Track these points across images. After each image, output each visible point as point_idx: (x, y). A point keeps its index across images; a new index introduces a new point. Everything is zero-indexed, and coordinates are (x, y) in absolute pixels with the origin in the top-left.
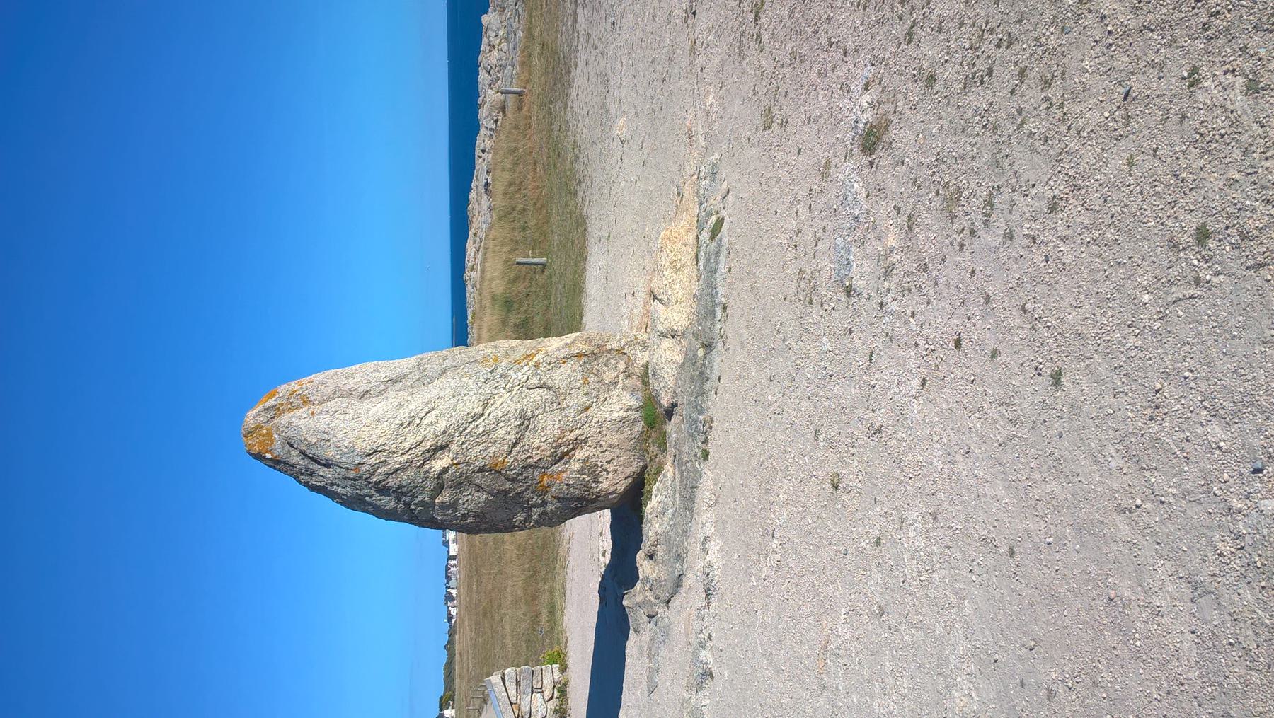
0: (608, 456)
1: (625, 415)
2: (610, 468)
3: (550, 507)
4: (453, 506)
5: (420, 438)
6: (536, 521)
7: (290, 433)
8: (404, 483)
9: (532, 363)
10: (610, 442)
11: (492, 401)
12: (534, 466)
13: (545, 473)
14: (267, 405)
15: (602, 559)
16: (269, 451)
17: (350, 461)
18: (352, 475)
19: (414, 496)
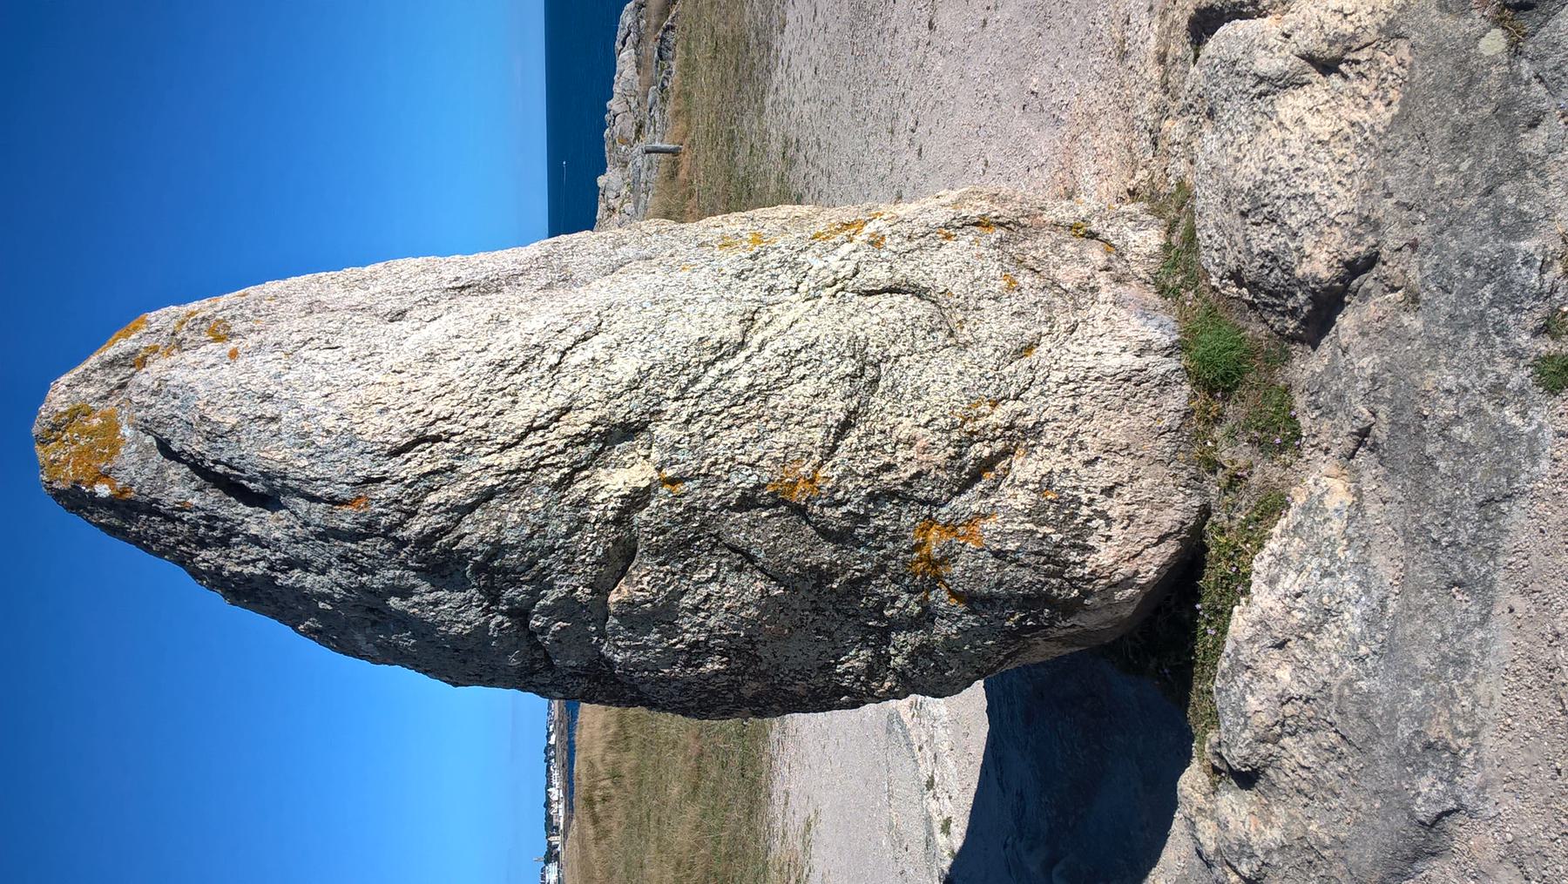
0: (1105, 474)
1: (1139, 363)
2: (1116, 507)
3: (944, 629)
4: (662, 615)
5: (561, 401)
6: (902, 675)
7: (162, 408)
8: (510, 538)
10: (1105, 436)
12: (901, 496)
13: (931, 520)
14: (109, 352)
15: (941, 839)
16: (104, 476)
17: (334, 474)
18: (346, 519)
19: (542, 582)
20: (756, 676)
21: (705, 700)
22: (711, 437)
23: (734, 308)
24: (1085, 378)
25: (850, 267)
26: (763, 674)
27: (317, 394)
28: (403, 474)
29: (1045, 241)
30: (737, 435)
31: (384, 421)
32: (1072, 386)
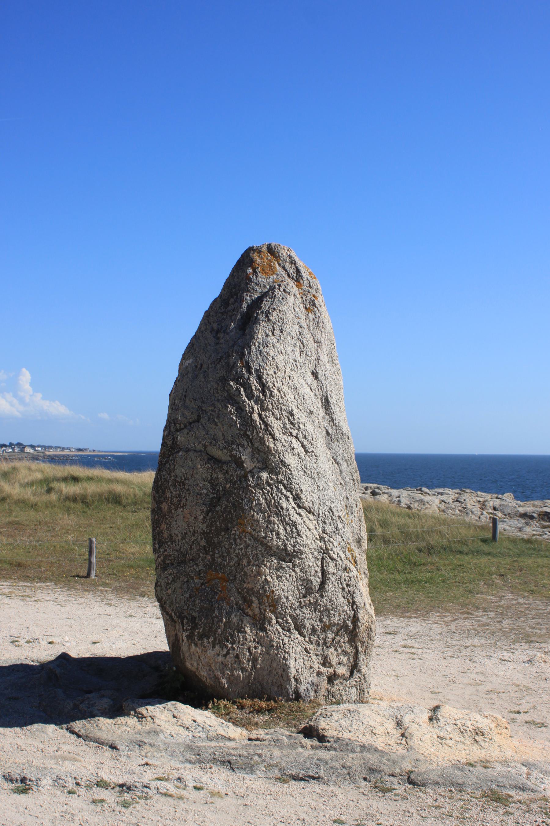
2: (230, 659)
9: (349, 564)
11: (311, 517)
20: (170, 508)
21: (161, 489)
22: (263, 491)
23: (315, 506)
24: (285, 652)
25: (335, 556)
26: (170, 511)
27: (283, 349)
28: (251, 379)
29: (348, 648)
30: (262, 501)
31: (271, 372)
32: (282, 646)
